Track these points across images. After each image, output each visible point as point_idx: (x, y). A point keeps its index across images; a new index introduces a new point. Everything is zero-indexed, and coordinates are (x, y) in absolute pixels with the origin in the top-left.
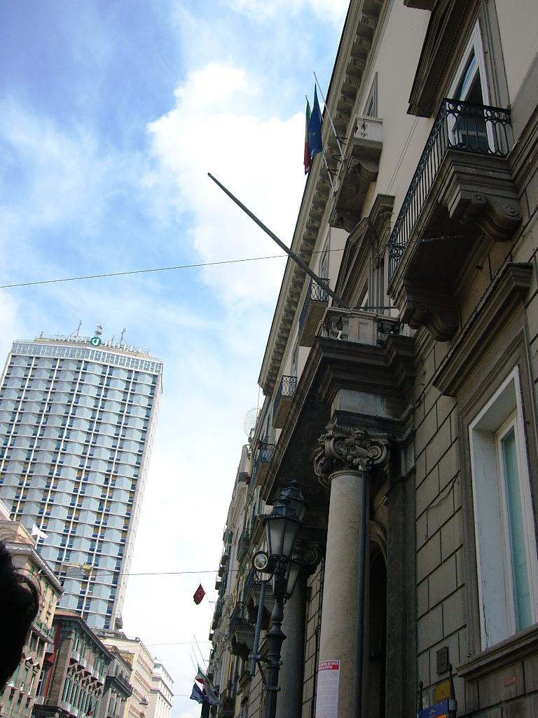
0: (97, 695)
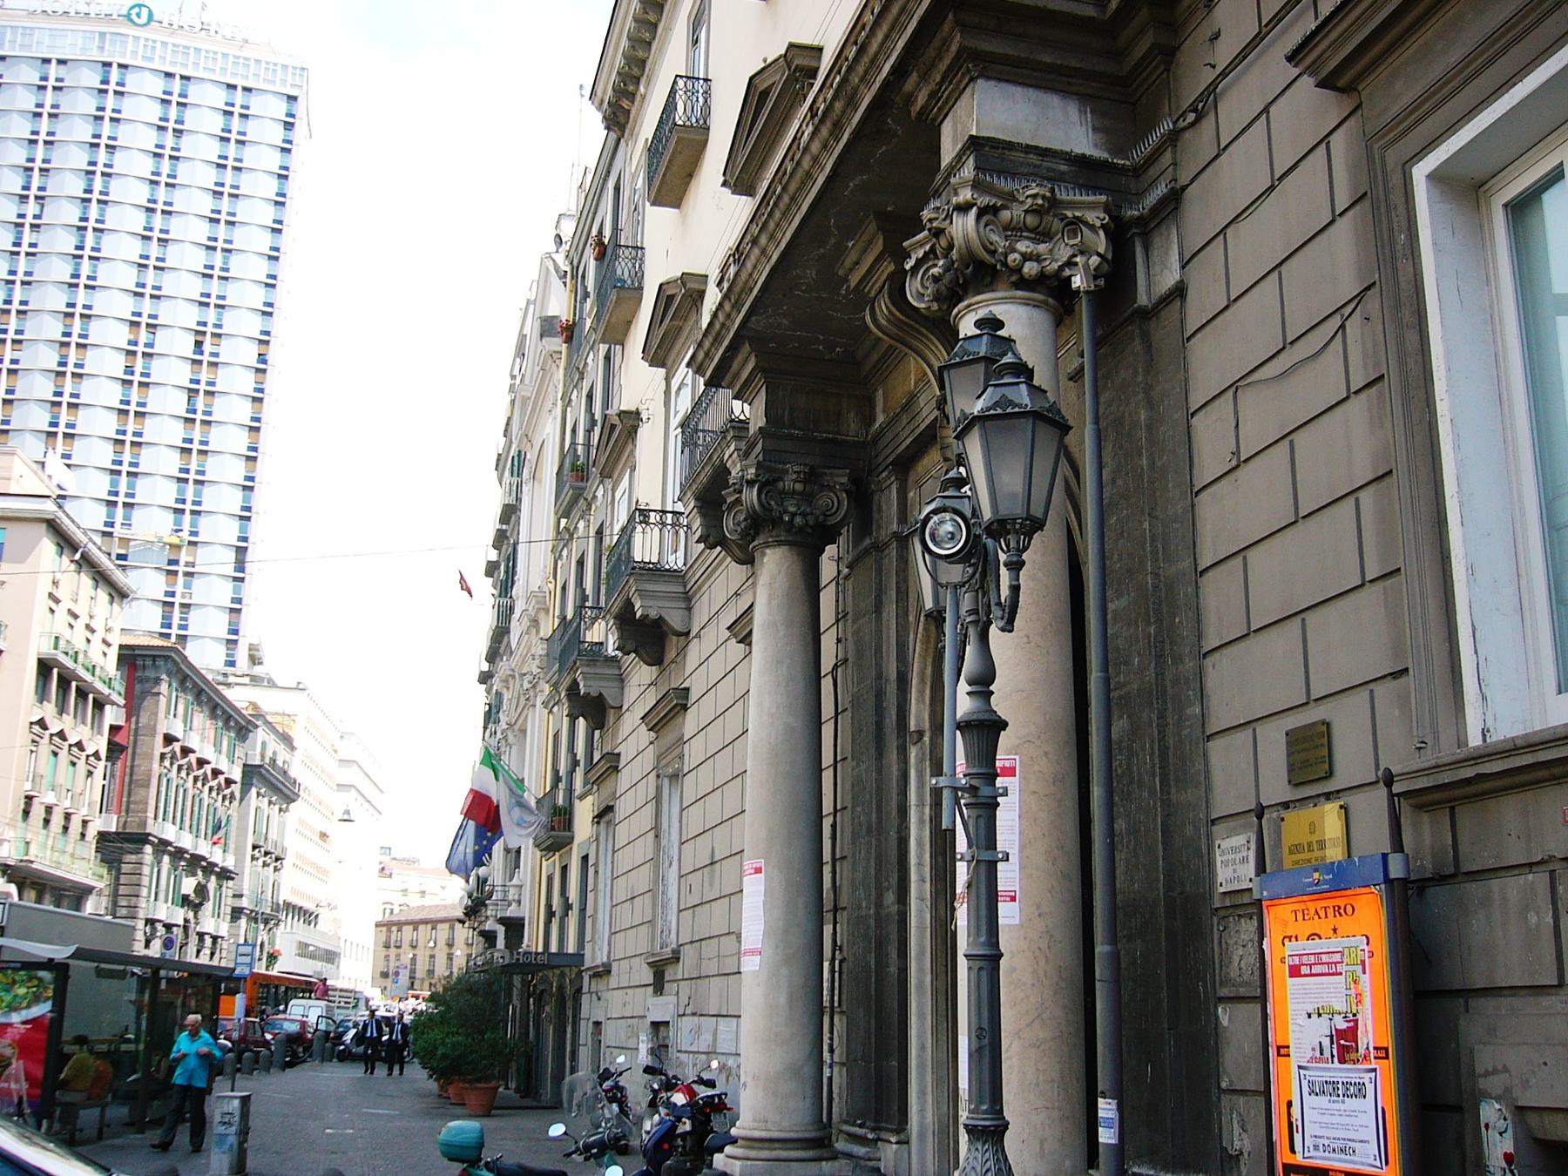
0: (227, 803)
